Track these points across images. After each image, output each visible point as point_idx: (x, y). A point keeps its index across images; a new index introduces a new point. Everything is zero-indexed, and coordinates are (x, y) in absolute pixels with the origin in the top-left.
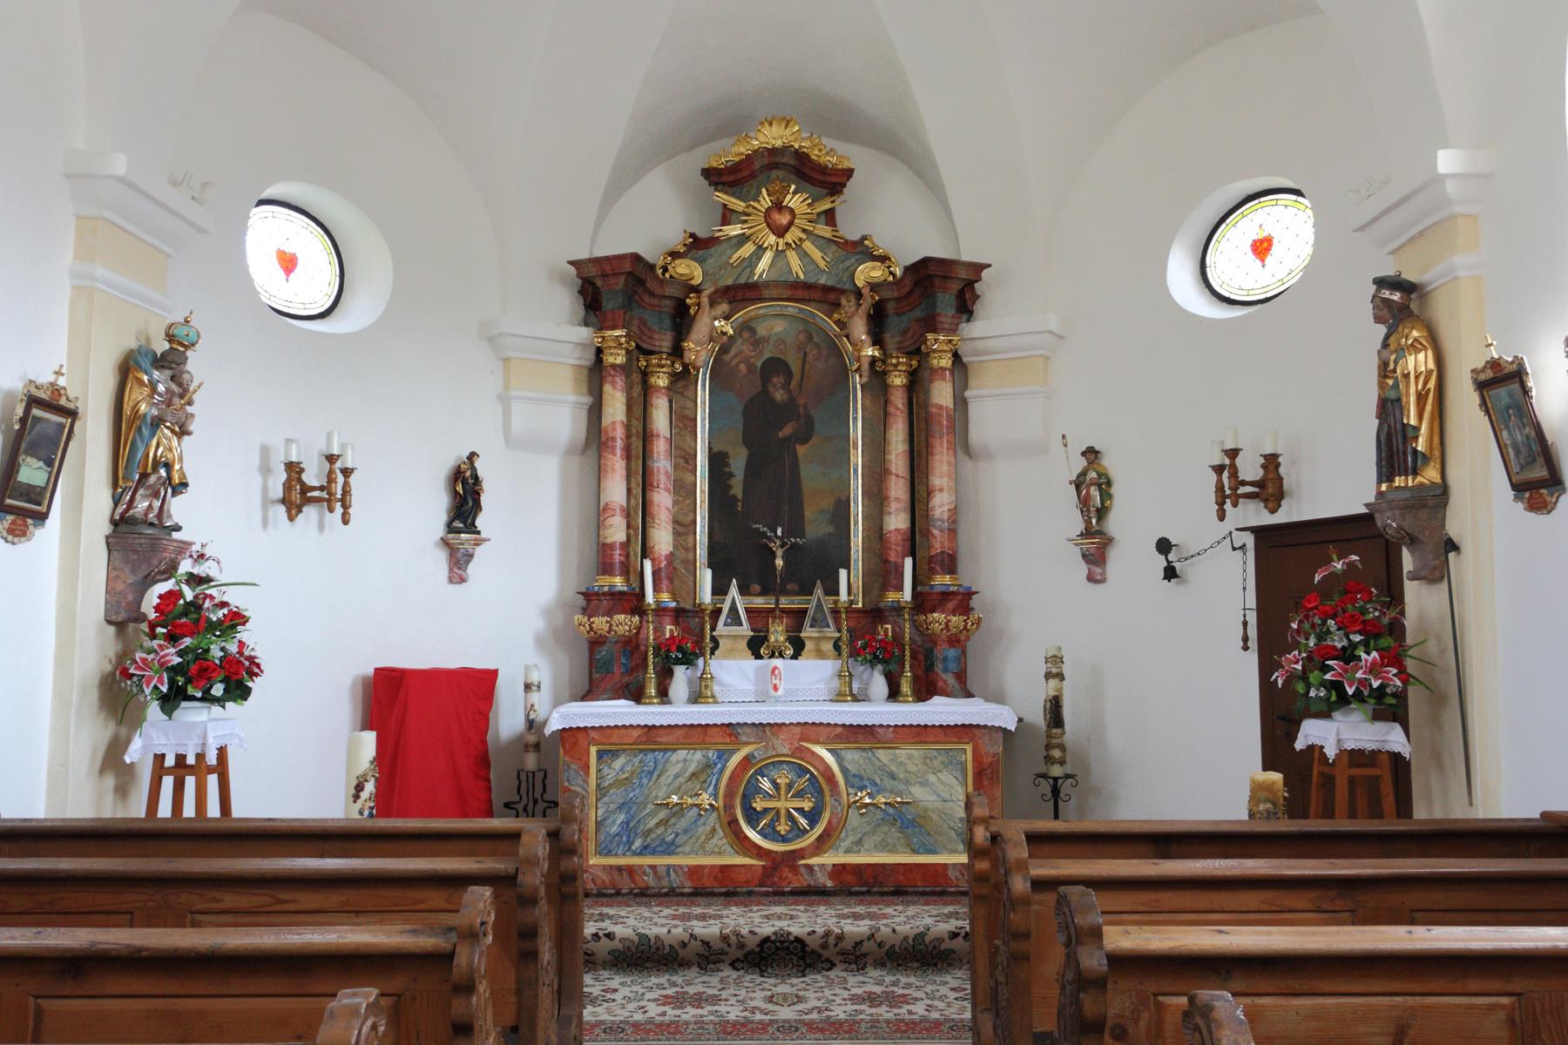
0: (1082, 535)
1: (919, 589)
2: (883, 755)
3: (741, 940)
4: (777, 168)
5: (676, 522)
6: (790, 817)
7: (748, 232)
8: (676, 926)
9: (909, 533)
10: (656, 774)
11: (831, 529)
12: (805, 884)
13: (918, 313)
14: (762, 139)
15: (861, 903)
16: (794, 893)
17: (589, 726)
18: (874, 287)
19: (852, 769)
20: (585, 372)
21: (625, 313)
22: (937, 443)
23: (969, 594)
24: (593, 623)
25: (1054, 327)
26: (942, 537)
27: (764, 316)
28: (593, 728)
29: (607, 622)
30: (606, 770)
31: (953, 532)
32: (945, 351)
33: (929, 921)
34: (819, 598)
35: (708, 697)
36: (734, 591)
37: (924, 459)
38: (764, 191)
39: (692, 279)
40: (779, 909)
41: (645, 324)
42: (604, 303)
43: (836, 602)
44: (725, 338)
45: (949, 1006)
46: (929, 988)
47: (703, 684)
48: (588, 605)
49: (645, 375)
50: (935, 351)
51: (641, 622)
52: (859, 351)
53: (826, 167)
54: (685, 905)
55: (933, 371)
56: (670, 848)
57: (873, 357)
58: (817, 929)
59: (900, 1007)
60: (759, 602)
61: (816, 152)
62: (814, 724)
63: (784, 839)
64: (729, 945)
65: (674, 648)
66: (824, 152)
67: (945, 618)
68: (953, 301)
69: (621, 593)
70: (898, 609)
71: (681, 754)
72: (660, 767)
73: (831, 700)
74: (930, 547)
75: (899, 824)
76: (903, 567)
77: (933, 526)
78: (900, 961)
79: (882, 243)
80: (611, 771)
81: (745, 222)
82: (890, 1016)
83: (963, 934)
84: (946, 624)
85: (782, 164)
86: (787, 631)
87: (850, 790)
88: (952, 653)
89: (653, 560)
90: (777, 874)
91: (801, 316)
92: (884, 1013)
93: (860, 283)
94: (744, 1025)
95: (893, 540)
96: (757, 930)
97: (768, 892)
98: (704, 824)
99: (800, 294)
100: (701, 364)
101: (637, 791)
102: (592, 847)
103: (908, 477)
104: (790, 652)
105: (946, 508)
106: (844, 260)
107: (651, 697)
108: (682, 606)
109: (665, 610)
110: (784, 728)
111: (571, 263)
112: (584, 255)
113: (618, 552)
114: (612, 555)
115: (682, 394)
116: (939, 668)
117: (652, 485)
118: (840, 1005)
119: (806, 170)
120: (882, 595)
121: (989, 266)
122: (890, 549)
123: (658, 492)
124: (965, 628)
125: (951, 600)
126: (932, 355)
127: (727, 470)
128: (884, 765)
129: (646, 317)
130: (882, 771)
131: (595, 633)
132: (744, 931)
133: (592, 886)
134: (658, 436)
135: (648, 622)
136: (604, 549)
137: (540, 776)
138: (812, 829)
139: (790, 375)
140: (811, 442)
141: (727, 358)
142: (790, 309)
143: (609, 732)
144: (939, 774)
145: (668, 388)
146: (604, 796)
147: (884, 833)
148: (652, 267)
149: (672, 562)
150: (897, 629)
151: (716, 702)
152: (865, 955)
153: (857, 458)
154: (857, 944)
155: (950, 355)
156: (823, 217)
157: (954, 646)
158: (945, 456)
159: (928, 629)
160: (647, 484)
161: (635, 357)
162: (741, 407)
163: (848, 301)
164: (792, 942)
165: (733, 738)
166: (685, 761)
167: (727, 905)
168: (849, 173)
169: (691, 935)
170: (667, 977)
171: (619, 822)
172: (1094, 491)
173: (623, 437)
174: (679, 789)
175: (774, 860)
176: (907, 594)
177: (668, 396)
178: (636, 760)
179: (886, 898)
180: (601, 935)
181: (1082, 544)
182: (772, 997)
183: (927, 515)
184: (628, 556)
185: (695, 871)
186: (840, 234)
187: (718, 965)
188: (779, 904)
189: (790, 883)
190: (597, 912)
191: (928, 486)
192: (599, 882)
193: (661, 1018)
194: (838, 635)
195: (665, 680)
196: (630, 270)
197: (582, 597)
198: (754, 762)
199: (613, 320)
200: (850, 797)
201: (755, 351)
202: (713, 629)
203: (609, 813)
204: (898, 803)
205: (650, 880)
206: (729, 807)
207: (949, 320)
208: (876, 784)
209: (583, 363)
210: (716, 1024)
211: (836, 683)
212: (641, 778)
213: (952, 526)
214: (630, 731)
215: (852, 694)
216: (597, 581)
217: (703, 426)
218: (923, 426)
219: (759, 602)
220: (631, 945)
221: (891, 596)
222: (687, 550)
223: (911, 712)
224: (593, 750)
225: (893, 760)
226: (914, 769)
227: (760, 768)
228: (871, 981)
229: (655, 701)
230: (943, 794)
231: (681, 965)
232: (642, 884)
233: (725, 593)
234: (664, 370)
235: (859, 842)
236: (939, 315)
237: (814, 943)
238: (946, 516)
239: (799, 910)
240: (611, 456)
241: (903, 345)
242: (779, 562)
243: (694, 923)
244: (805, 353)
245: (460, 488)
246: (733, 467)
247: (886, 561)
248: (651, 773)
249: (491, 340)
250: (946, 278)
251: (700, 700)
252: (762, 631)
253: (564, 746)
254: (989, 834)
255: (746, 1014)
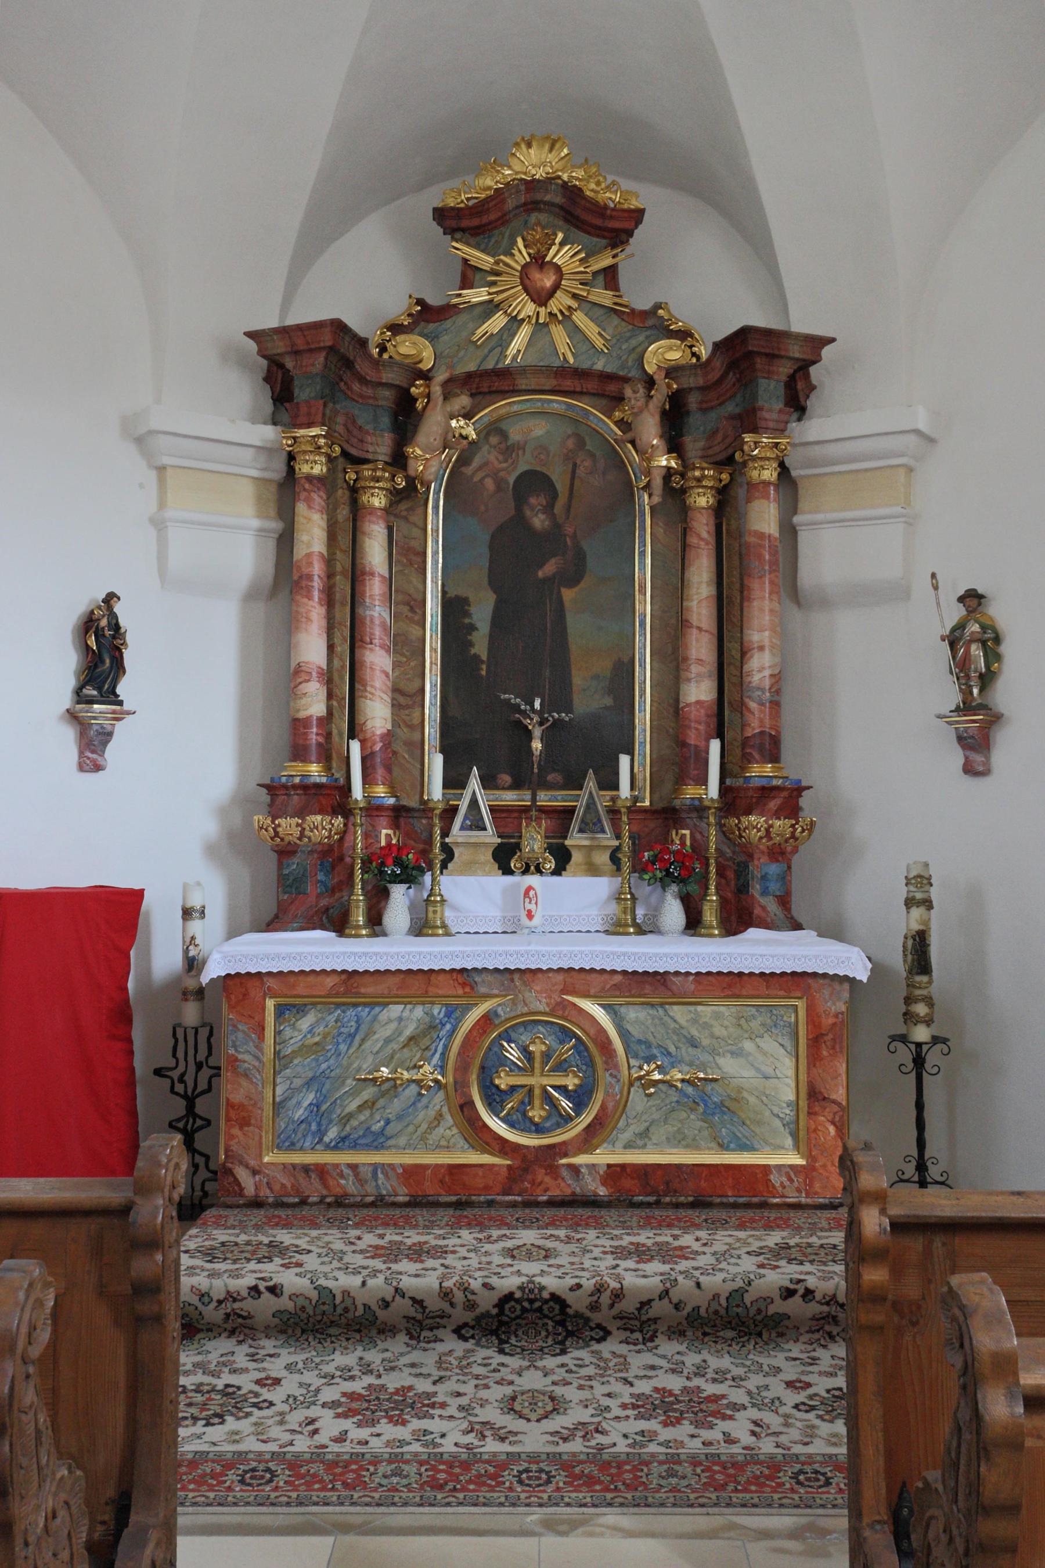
0: (958, 709)
1: (728, 782)
2: (679, 1013)
3: (470, 1297)
4: (540, 210)
5: (396, 690)
6: (548, 1098)
7: (498, 298)
8: (375, 1273)
9: (715, 707)
10: (358, 1038)
11: (608, 701)
12: (568, 1191)
13: (731, 408)
14: (518, 167)
15: (647, 1223)
16: (551, 1203)
17: (264, 971)
18: (672, 371)
19: (635, 1032)
20: (273, 488)
21: (325, 405)
22: (755, 584)
23: (798, 790)
24: (279, 825)
25: (922, 426)
26: (761, 711)
27: (517, 414)
28: (270, 974)
29: (298, 825)
30: (288, 1032)
31: (776, 705)
32: (768, 459)
33: (748, 1264)
34: (591, 793)
35: (437, 927)
36: (474, 784)
37: (737, 608)
38: (520, 240)
39: (420, 361)
40: (528, 1236)
41: (354, 422)
42: (296, 391)
43: (614, 799)
44: (465, 442)
45: (787, 1425)
46: (755, 1381)
47: (431, 909)
48: (273, 801)
49: (354, 491)
50: (754, 459)
51: (345, 825)
52: (649, 460)
53: (606, 207)
54: (396, 1225)
55: (752, 486)
56: (377, 1141)
57: (668, 468)
58: (583, 1282)
59: (711, 1426)
60: (509, 798)
61: (593, 186)
62: (582, 970)
63: (538, 1129)
64: (452, 1305)
65: (390, 861)
66: (603, 185)
67: (766, 822)
68: (781, 391)
69: (318, 786)
70: (699, 809)
71: (395, 1010)
72: (364, 1028)
73: (607, 932)
74: (744, 726)
75: (701, 1109)
76: (707, 753)
77: (749, 697)
78: (707, 1330)
79: (683, 314)
80: (296, 1034)
81: (493, 284)
82: (695, 1446)
83: (801, 1291)
84: (767, 831)
85: (545, 203)
86: (547, 837)
87: (633, 1062)
88: (774, 869)
89: (363, 742)
90: (529, 1177)
91: (569, 413)
92: (687, 1440)
93: (650, 369)
94: (466, 1466)
95: (692, 717)
96: (494, 1281)
97: (515, 1201)
98: (427, 1107)
99: (568, 384)
100: (431, 477)
101: (332, 1061)
102: (267, 1138)
103: (715, 631)
104: (550, 865)
105: (767, 673)
106: (630, 338)
107: (358, 927)
108: (402, 803)
109: (380, 808)
110: (540, 975)
111: (250, 335)
112: (271, 321)
113: (314, 730)
114: (306, 734)
115: (406, 519)
116: (756, 889)
117: (362, 641)
118: (617, 1418)
119: (578, 212)
120: (676, 791)
121: (833, 340)
122: (689, 727)
123: (371, 650)
124: (793, 836)
125: (774, 798)
126: (751, 464)
127: (467, 621)
128: (682, 1028)
129: (356, 412)
130: (678, 1035)
131: (282, 840)
132: (475, 1285)
133: (268, 1192)
134: (372, 574)
135: (354, 825)
136: (299, 725)
137: (204, 1033)
138: (578, 1114)
139: (554, 495)
140: (582, 585)
141: (468, 470)
142: (555, 405)
143: (292, 979)
144: (758, 1040)
145: (387, 511)
146: (286, 1067)
147: (680, 1121)
148: (363, 343)
149: (390, 743)
150: (698, 836)
151: (448, 934)
152: (655, 1320)
153: (645, 606)
154: (643, 1304)
155: (775, 465)
156: (601, 278)
157: (777, 861)
158: (767, 602)
159: (741, 836)
160: (356, 640)
161: (340, 467)
162: (488, 537)
163: (635, 392)
164: (546, 1301)
165: (467, 989)
166: (400, 1019)
167: (456, 1225)
168: (638, 215)
169: (397, 1289)
170: (359, 1352)
171: (306, 1104)
172: (976, 651)
173: (323, 575)
174: (392, 1057)
175: (524, 1159)
176: (713, 789)
177: (387, 522)
178: (332, 1018)
179: (682, 1213)
180: (262, 1288)
181: (958, 722)
182: (514, 1399)
183: (741, 683)
184: (328, 736)
185: (412, 1173)
186: (624, 300)
187: (435, 1332)
188: (527, 1224)
189: (546, 1190)
190: (266, 1240)
191: (742, 643)
192: (277, 1187)
193: (335, 1448)
194: (616, 843)
195: (379, 902)
196: (329, 343)
197: (265, 791)
198: (497, 1022)
199: (309, 414)
200: (633, 1071)
201: (506, 461)
202: (445, 833)
203: (293, 1091)
204: (700, 1079)
205: (349, 1185)
206: (461, 1085)
207: (775, 416)
208: (669, 1054)
209: (267, 475)
210: (421, 1463)
211: (613, 908)
212: (338, 1044)
213: (776, 698)
214: (320, 978)
215: (635, 924)
216: (285, 768)
217: (435, 562)
218: (737, 562)
219: (509, 798)
220: (306, 1303)
221: (691, 792)
222: (411, 727)
223: (720, 954)
224: (270, 1004)
225: (694, 1021)
226: (725, 1033)
227: (506, 1030)
228: (663, 1363)
229: (364, 932)
230: (763, 1068)
231: (381, 1332)
232: (338, 1191)
233: (462, 785)
234: (380, 484)
235: (645, 1134)
236: (761, 409)
237: (578, 1303)
238: (767, 684)
239: (557, 1238)
240: (305, 600)
241: (710, 452)
242: (537, 745)
243: (405, 1265)
244: (575, 465)
245: (92, 642)
246: (475, 617)
247: (683, 744)
248: (352, 1036)
249: (139, 441)
250: (772, 357)
251: (425, 931)
252: (513, 837)
253: (228, 998)
254: (886, 1221)
255: (470, 1438)
